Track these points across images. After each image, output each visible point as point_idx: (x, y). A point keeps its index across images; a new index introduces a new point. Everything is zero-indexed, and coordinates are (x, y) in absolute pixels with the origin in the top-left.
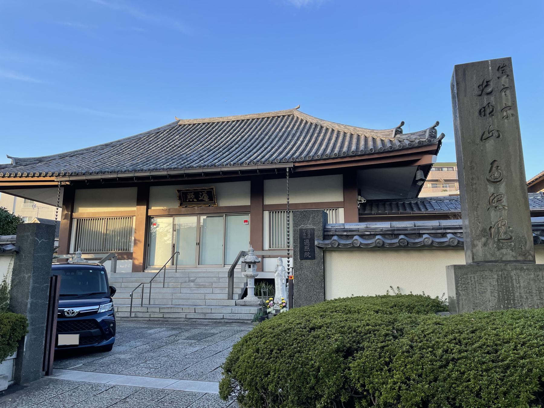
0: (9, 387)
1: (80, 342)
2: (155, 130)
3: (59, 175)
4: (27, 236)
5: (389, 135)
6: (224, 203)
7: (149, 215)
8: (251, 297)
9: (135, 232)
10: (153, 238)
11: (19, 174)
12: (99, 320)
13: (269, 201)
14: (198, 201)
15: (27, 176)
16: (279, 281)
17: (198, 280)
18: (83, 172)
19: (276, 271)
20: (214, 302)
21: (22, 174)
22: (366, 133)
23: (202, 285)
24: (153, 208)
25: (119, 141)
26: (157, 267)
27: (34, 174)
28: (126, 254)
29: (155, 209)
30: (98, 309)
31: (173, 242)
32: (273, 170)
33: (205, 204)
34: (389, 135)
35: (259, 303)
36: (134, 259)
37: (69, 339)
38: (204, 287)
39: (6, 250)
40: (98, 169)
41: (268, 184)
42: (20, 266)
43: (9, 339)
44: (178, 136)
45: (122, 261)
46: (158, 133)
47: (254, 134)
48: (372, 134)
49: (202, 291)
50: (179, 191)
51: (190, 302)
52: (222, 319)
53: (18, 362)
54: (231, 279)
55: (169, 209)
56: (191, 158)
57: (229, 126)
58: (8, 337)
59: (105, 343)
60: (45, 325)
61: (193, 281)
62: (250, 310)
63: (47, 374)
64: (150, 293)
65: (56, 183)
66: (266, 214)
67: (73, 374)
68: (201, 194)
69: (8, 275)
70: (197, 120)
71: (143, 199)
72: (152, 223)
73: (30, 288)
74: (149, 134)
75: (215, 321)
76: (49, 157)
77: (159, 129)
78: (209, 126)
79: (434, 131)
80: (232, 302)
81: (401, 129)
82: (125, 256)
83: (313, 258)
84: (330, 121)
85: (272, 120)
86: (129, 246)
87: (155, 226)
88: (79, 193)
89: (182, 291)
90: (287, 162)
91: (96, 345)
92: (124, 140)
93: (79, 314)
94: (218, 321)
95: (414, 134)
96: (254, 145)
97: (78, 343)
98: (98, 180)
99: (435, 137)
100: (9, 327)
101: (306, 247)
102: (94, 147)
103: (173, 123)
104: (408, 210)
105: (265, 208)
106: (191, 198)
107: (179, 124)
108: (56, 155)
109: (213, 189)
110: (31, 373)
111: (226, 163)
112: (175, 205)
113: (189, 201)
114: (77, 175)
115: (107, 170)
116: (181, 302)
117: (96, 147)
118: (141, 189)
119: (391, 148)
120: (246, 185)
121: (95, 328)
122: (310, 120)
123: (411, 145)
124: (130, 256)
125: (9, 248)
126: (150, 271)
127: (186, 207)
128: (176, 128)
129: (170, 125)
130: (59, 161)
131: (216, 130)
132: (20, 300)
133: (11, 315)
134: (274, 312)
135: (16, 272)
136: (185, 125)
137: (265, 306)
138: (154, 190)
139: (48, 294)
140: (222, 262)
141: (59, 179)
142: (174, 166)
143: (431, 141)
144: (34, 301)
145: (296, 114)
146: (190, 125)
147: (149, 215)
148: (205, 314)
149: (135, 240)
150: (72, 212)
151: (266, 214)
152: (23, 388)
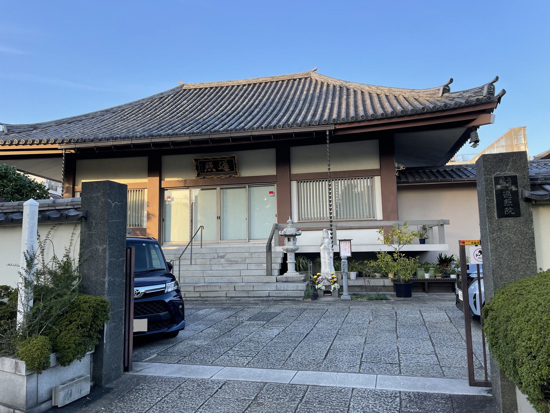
0: (92, 388)
1: (148, 329)
2: (158, 95)
3: (62, 142)
4: (98, 197)
5: (435, 94)
6: (246, 173)
8: (291, 272)
9: (148, 206)
10: (167, 210)
11: (16, 141)
12: (167, 300)
13: (296, 170)
14: (218, 171)
15: (25, 144)
16: (326, 254)
17: (228, 256)
18: (91, 138)
19: (322, 244)
20: (252, 279)
21: (19, 141)
22: (405, 93)
25: (120, 107)
26: (174, 243)
27: (33, 141)
28: (138, 229)
29: (168, 180)
30: (165, 288)
32: (311, 133)
33: (225, 174)
34: (435, 94)
35: (303, 278)
37: (140, 325)
38: (237, 263)
39: (69, 216)
40: (107, 135)
41: (295, 151)
42: (90, 236)
43: (90, 329)
44: (185, 101)
46: (162, 98)
47: (272, 97)
48: (413, 93)
49: (236, 267)
50: (196, 160)
51: (225, 280)
52: (267, 297)
53: (97, 359)
54: (269, 253)
55: (185, 181)
56: (211, 122)
57: (241, 90)
58: (89, 327)
59: (175, 328)
60: (124, 309)
61: (222, 257)
62: (298, 286)
63: (126, 369)
64: (179, 271)
65: (60, 152)
66: (294, 184)
67: (154, 367)
69: (71, 248)
70: (203, 84)
71: (155, 169)
73: (107, 262)
74: (152, 99)
75: (261, 299)
76: (45, 124)
77: (162, 94)
78: (218, 91)
79: (492, 87)
80: (273, 279)
81: (448, 87)
83: (518, 214)
84: (356, 80)
85: (288, 84)
86: (142, 221)
88: (80, 163)
89: (213, 268)
90: (327, 124)
91: (165, 330)
92: (126, 105)
93: (145, 295)
94: (265, 299)
95: (467, 91)
96: (278, 108)
97: (146, 331)
98: (109, 148)
99: (493, 94)
100: (90, 314)
101: (506, 201)
102: (93, 113)
103: (177, 88)
104: (448, 178)
105: (291, 178)
106: (210, 168)
107: (183, 88)
108: (52, 122)
109: (234, 157)
110: (113, 370)
111: (254, 125)
112: (193, 176)
113: (207, 171)
114: (84, 141)
115: (118, 136)
116: (214, 280)
117: (96, 113)
118: (154, 157)
119: (446, 107)
120: (271, 153)
121: (164, 311)
122: (332, 82)
123: (468, 103)
125: (73, 213)
126: (167, 248)
127: (204, 178)
128: (180, 93)
129: (174, 90)
130: (56, 128)
131: (227, 94)
132: (94, 279)
133: (89, 298)
134: (324, 288)
135: (85, 244)
136: (190, 90)
137: (314, 283)
138: (167, 160)
139: (125, 271)
140: (245, 236)
141: (63, 147)
142: (195, 130)
143: (490, 98)
144: (112, 280)
145: (315, 76)
146: (195, 89)
148: (248, 291)
149: (148, 214)
150: (74, 185)
152: (108, 391)
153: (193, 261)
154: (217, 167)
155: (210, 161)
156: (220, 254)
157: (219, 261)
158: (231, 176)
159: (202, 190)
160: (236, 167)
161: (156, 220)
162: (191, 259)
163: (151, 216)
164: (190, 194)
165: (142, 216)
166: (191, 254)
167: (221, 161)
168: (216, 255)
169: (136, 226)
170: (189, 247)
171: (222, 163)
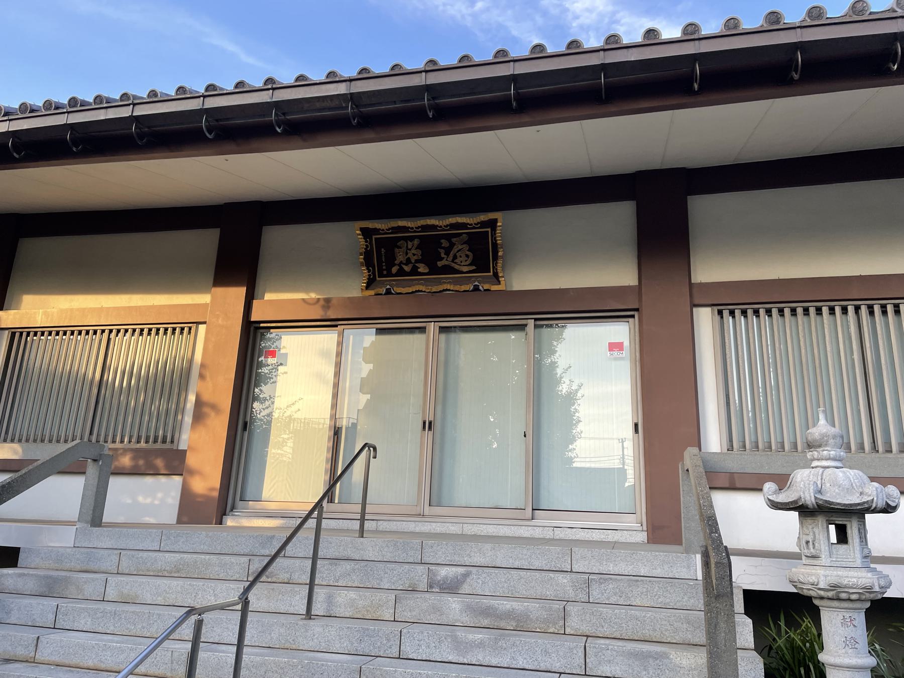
7: (254, 317)
9: (202, 376)
13: (708, 270)
14: (434, 270)
17: (477, 583)
23: (509, 615)
24: (268, 296)
26: (272, 506)
28: (162, 453)
29: (274, 300)
31: (334, 417)
36: (192, 472)
41: (704, 209)
45: (149, 480)
50: (366, 232)
55: (328, 301)
61: (451, 587)
66: (704, 318)
68: (445, 243)
72: (260, 350)
82: (159, 463)
86: (177, 427)
87: (271, 361)
105: (702, 296)
106: (408, 261)
112: (351, 287)
113: (401, 273)
120: (621, 215)
124: (174, 462)
127: (388, 292)
138: (275, 238)
147: (254, 317)
149: (199, 403)
151: (704, 318)
153: (320, 594)
154: (433, 255)
155: (412, 239)
156: (443, 572)
157: (436, 609)
158: (476, 289)
159: (380, 331)
160: (496, 258)
161: (219, 425)
162: (312, 585)
163: (206, 410)
164: (340, 344)
165: (180, 409)
166: (315, 558)
167: (448, 237)
168: (420, 575)
169: (155, 441)
170: (312, 523)
171: (452, 245)
